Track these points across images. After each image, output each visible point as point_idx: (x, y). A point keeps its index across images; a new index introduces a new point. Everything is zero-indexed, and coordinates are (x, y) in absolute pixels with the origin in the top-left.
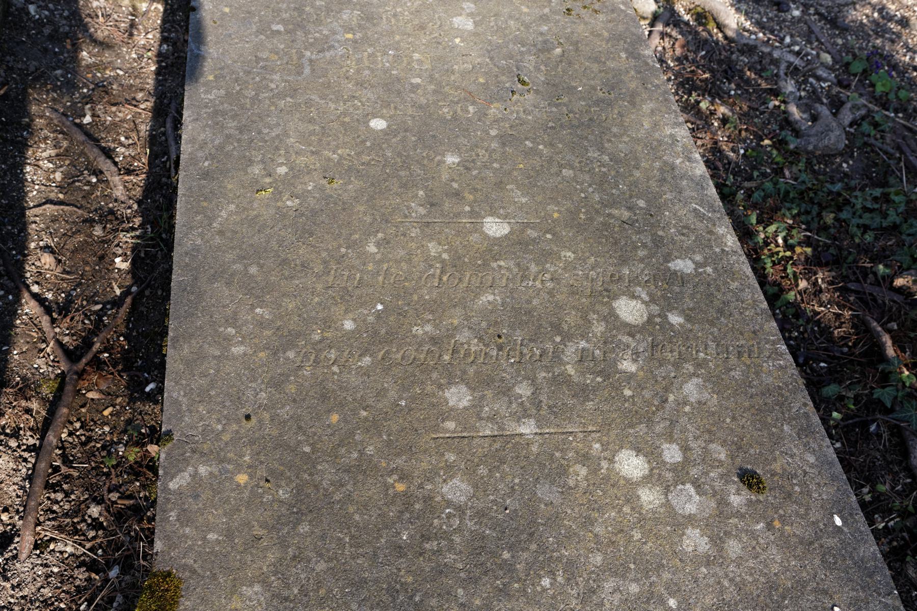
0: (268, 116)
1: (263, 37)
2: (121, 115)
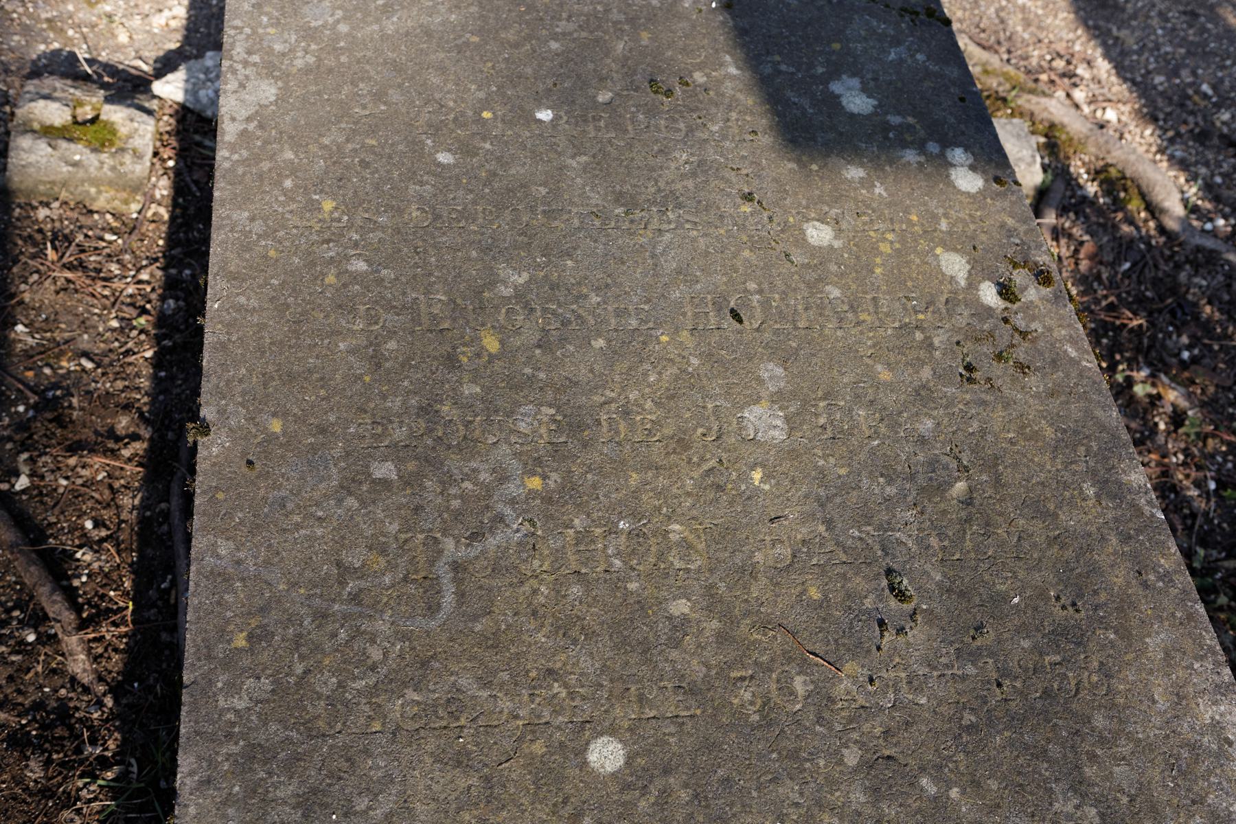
0: (367, 752)
1: (351, 502)
2: (85, 473)
